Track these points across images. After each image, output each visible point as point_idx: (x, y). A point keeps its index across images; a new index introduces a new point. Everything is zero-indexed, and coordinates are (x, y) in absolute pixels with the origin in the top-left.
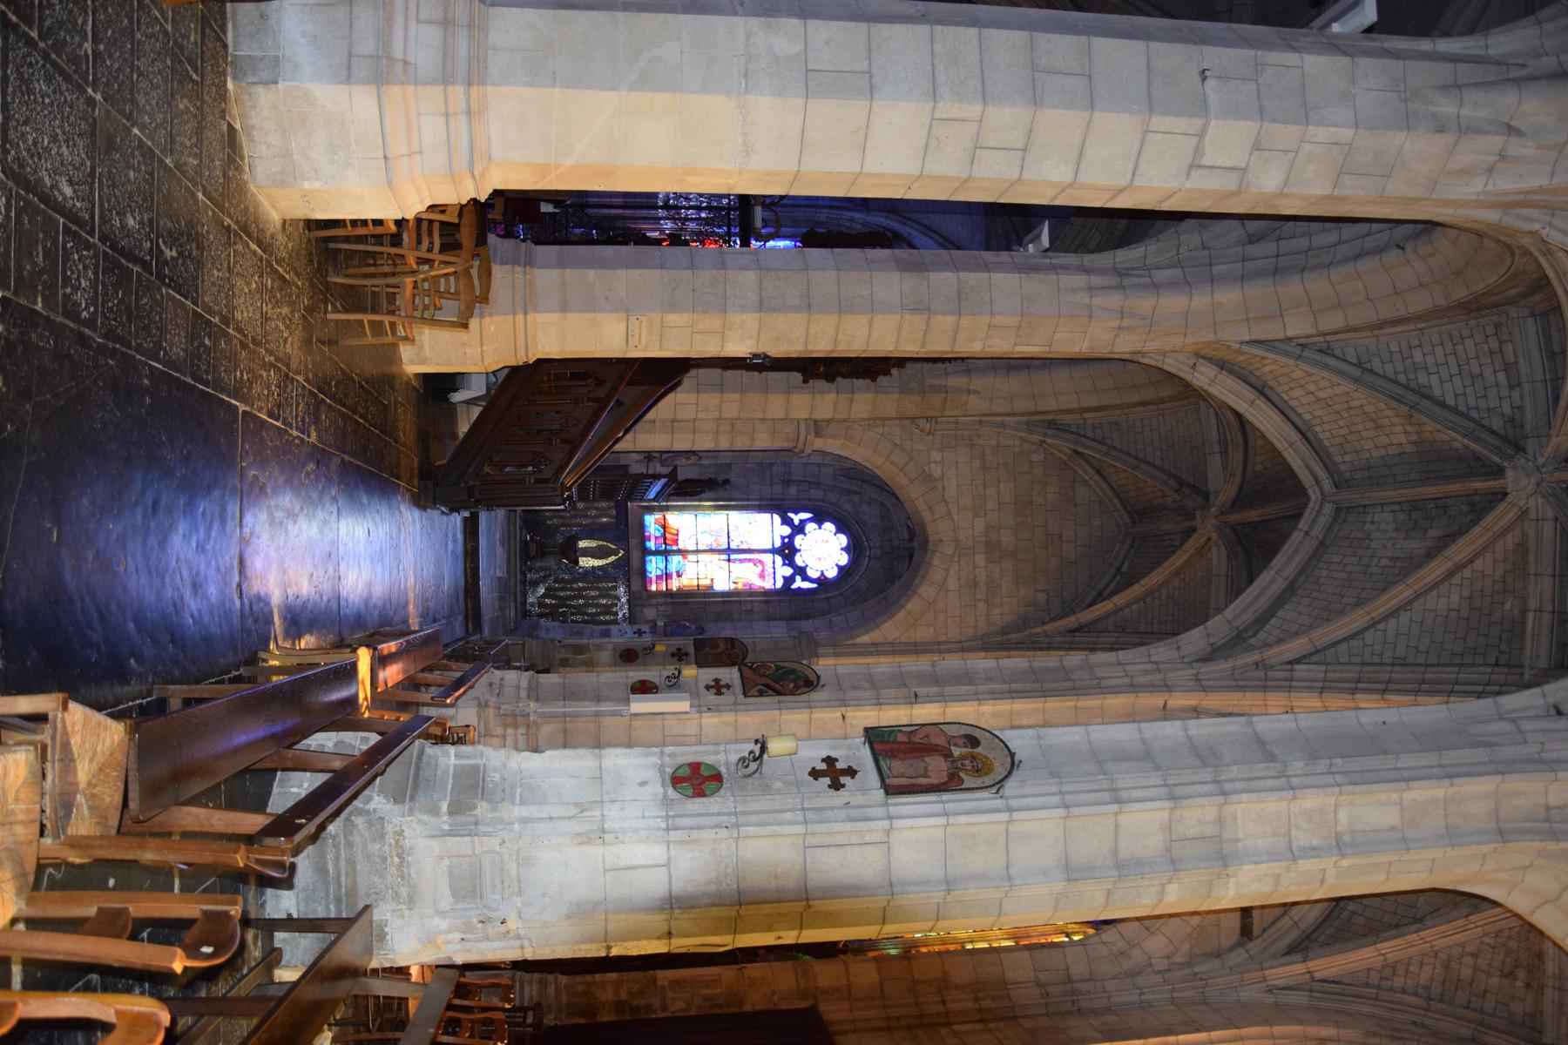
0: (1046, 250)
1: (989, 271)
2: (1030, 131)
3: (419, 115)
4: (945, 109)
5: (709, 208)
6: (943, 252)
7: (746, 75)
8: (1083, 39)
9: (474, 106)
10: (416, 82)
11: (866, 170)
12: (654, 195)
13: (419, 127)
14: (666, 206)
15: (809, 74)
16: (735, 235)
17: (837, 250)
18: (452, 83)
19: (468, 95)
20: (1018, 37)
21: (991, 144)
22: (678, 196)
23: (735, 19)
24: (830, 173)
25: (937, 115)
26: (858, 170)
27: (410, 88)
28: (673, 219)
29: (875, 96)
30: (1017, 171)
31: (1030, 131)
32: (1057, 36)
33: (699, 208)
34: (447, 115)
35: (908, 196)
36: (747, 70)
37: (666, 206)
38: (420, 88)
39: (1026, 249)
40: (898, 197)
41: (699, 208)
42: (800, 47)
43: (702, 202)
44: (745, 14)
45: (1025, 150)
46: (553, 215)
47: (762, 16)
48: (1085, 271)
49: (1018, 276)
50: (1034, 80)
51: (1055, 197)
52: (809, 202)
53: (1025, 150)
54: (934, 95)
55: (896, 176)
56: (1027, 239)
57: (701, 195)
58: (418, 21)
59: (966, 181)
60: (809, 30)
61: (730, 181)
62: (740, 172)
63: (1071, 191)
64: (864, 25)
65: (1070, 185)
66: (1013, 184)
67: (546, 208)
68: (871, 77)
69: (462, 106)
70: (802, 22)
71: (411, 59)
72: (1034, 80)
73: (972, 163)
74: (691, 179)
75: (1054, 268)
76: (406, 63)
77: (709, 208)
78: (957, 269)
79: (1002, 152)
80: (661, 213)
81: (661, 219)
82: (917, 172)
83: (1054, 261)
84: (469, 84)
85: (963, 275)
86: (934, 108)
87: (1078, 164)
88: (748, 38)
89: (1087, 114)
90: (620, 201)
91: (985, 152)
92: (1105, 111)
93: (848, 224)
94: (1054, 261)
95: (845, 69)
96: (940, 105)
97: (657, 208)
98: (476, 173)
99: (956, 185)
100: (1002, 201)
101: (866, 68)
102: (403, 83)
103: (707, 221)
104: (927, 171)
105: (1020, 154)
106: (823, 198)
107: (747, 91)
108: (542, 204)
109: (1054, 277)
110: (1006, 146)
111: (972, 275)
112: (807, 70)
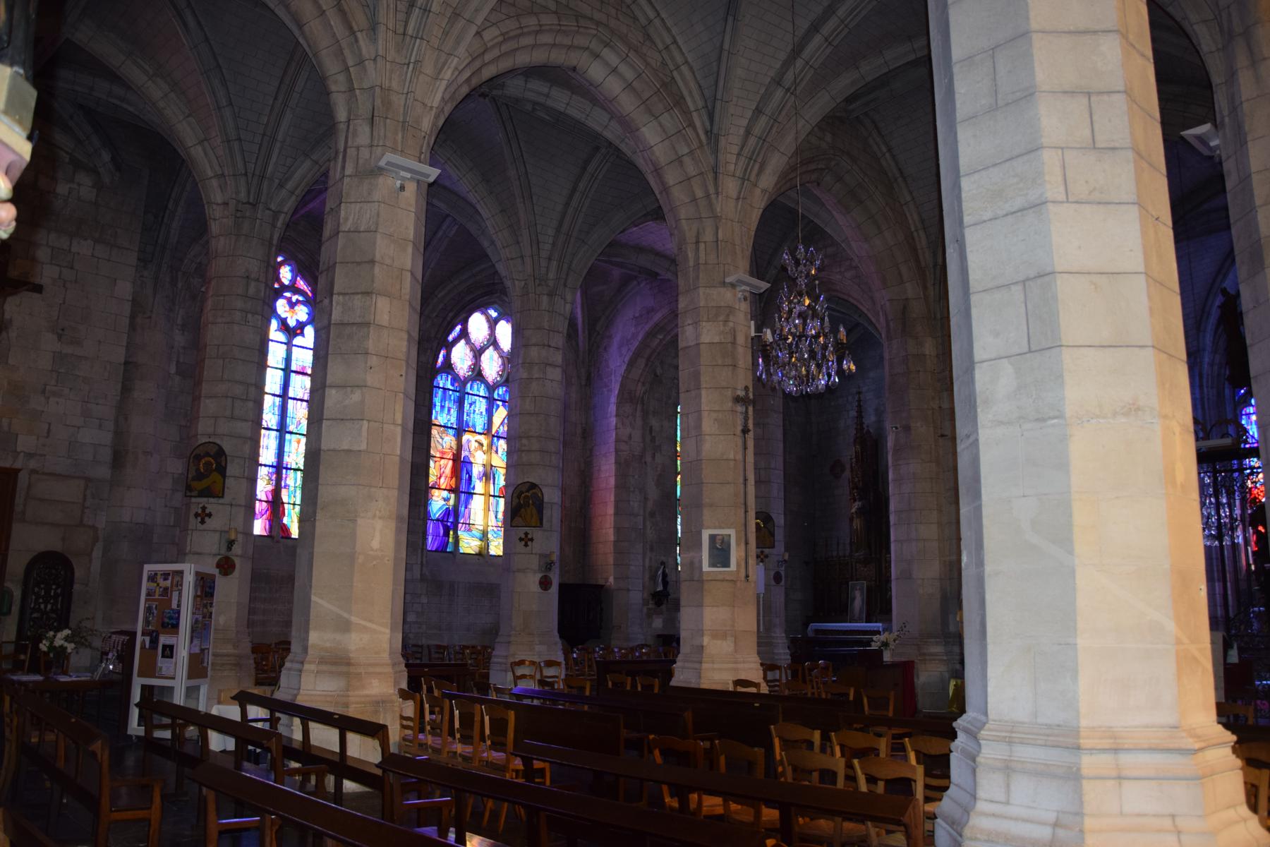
0: (1215, 125)
1: (1250, 175)
2: (1065, 92)
3: (1121, 814)
4: (1053, 189)
5: (1217, 494)
6: (1237, 259)
7: (1043, 420)
8: (956, 69)
9: (1106, 743)
10: (1080, 814)
11: (1142, 269)
12: (1208, 550)
13: (1139, 815)
14: (1219, 537)
15: (1033, 348)
16: (1241, 464)
17: (1248, 341)
18: (1079, 769)
19: (1092, 750)
20: (964, 134)
21: (1087, 132)
22: (1206, 526)
23: (982, 439)
24: (1151, 309)
25: (1062, 197)
26: (1142, 277)
27: (1088, 823)
28: (1233, 529)
29: (1049, 269)
30: (1116, 97)
31: (1065, 92)
32: (957, 96)
33: (1218, 505)
34: (1120, 778)
35: (1169, 222)
36: (1037, 420)
37: (1219, 537)
38: (1087, 809)
39: (1217, 147)
40: (1171, 233)
41: (1218, 505)
42: (1005, 362)
43: (1211, 503)
44: (976, 431)
45: (1089, 94)
46: (1239, 649)
47: (976, 411)
48: (1232, 75)
49: (1250, 144)
50: (1007, 104)
51: (1143, 55)
52: (1199, 406)
53: (1089, 94)
54: (1038, 206)
55: (1144, 233)
56: (1206, 152)
57: (1203, 504)
58: (1007, 803)
59: (1138, 153)
60: (985, 357)
61: (1177, 430)
62: (1165, 417)
63: (1131, 37)
64: (974, 299)
65: (1125, 36)
66: (1134, 101)
67: (1234, 657)
68: (1028, 279)
69: (1106, 758)
70: (977, 366)
71: (1051, 817)
72: (1007, 104)
73: (1114, 149)
74: (1180, 477)
75: (1234, 109)
76: (1056, 825)
77: (1217, 494)
78: (1253, 209)
79: (1095, 118)
80: (1227, 541)
81: (1233, 543)
82: (1136, 208)
83: (1226, 113)
84: (1078, 748)
85: (1258, 202)
86: (1053, 202)
87: (1095, 32)
88: (1001, 423)
89: (1035, 36)
90: (1197, 391)
91: (1098, 138)
92: (1028, 18)
93: (1216, 368)
94: (1226, 113)
95: (1023, 310)
96: (1049, 195)
97: (1221, 546)
98: (1197, 746)
99: (1145, 165)
100: (1157, 115)
101: (1019, 287)
102: (1081, 831)
103: (1230, 495)
104: (1133, 198)
105: (1093, 98)
106: (1193, 393)
107: (1061, 416)
108: (535, 762)
109: (1245, 105)
110: (1087, 116)
111: (1256, 192)
112: (1030, 351)
